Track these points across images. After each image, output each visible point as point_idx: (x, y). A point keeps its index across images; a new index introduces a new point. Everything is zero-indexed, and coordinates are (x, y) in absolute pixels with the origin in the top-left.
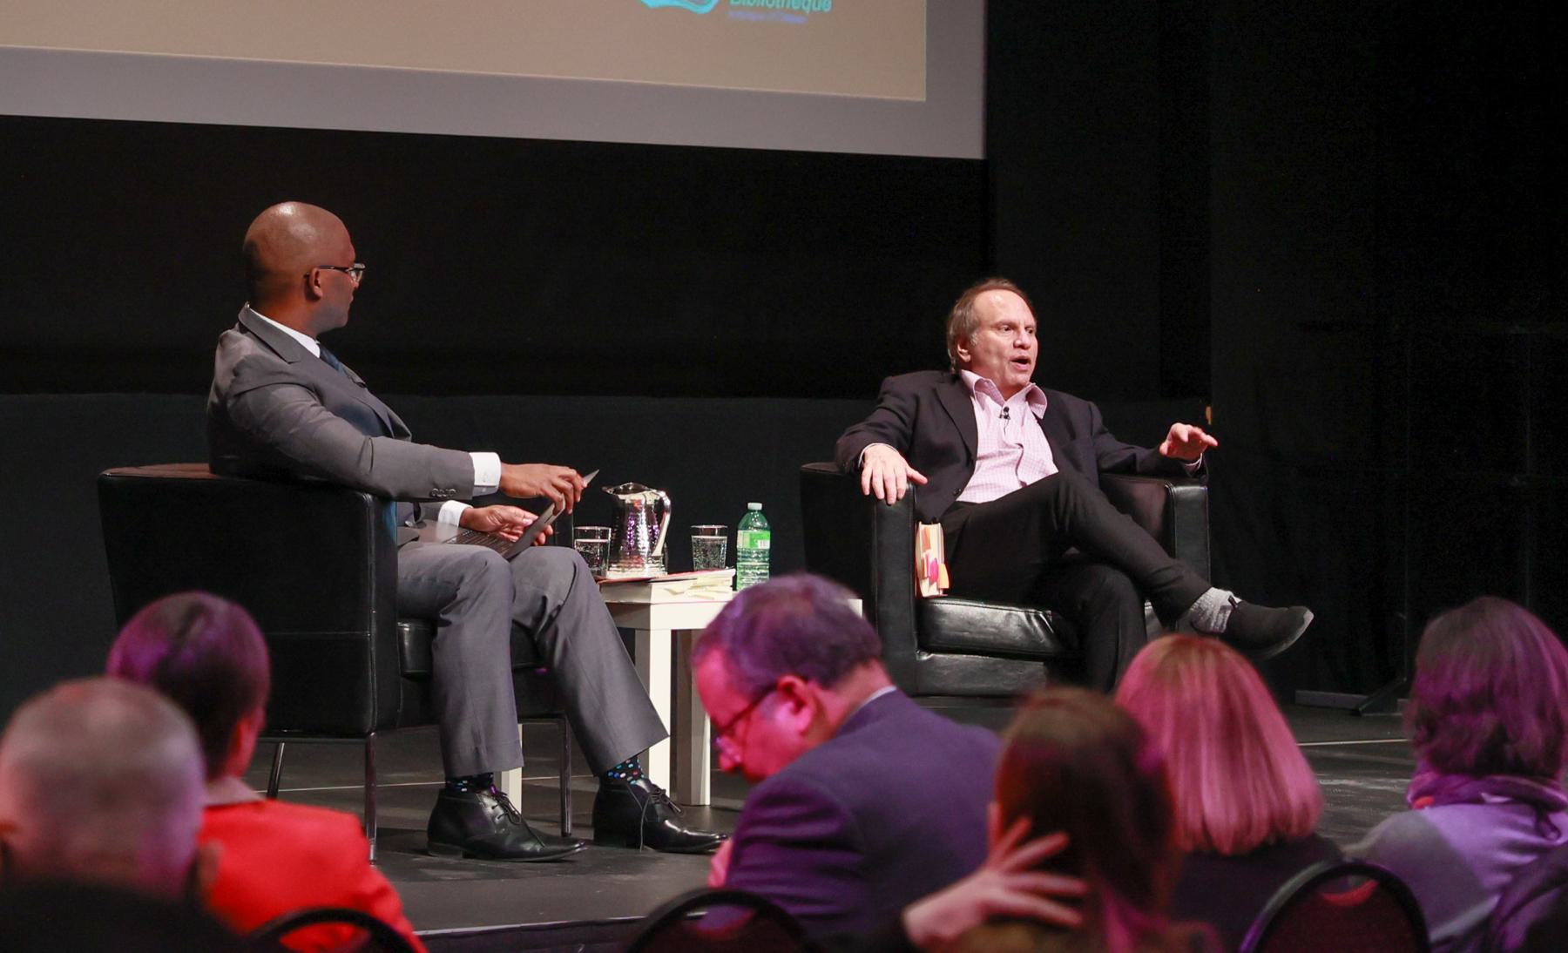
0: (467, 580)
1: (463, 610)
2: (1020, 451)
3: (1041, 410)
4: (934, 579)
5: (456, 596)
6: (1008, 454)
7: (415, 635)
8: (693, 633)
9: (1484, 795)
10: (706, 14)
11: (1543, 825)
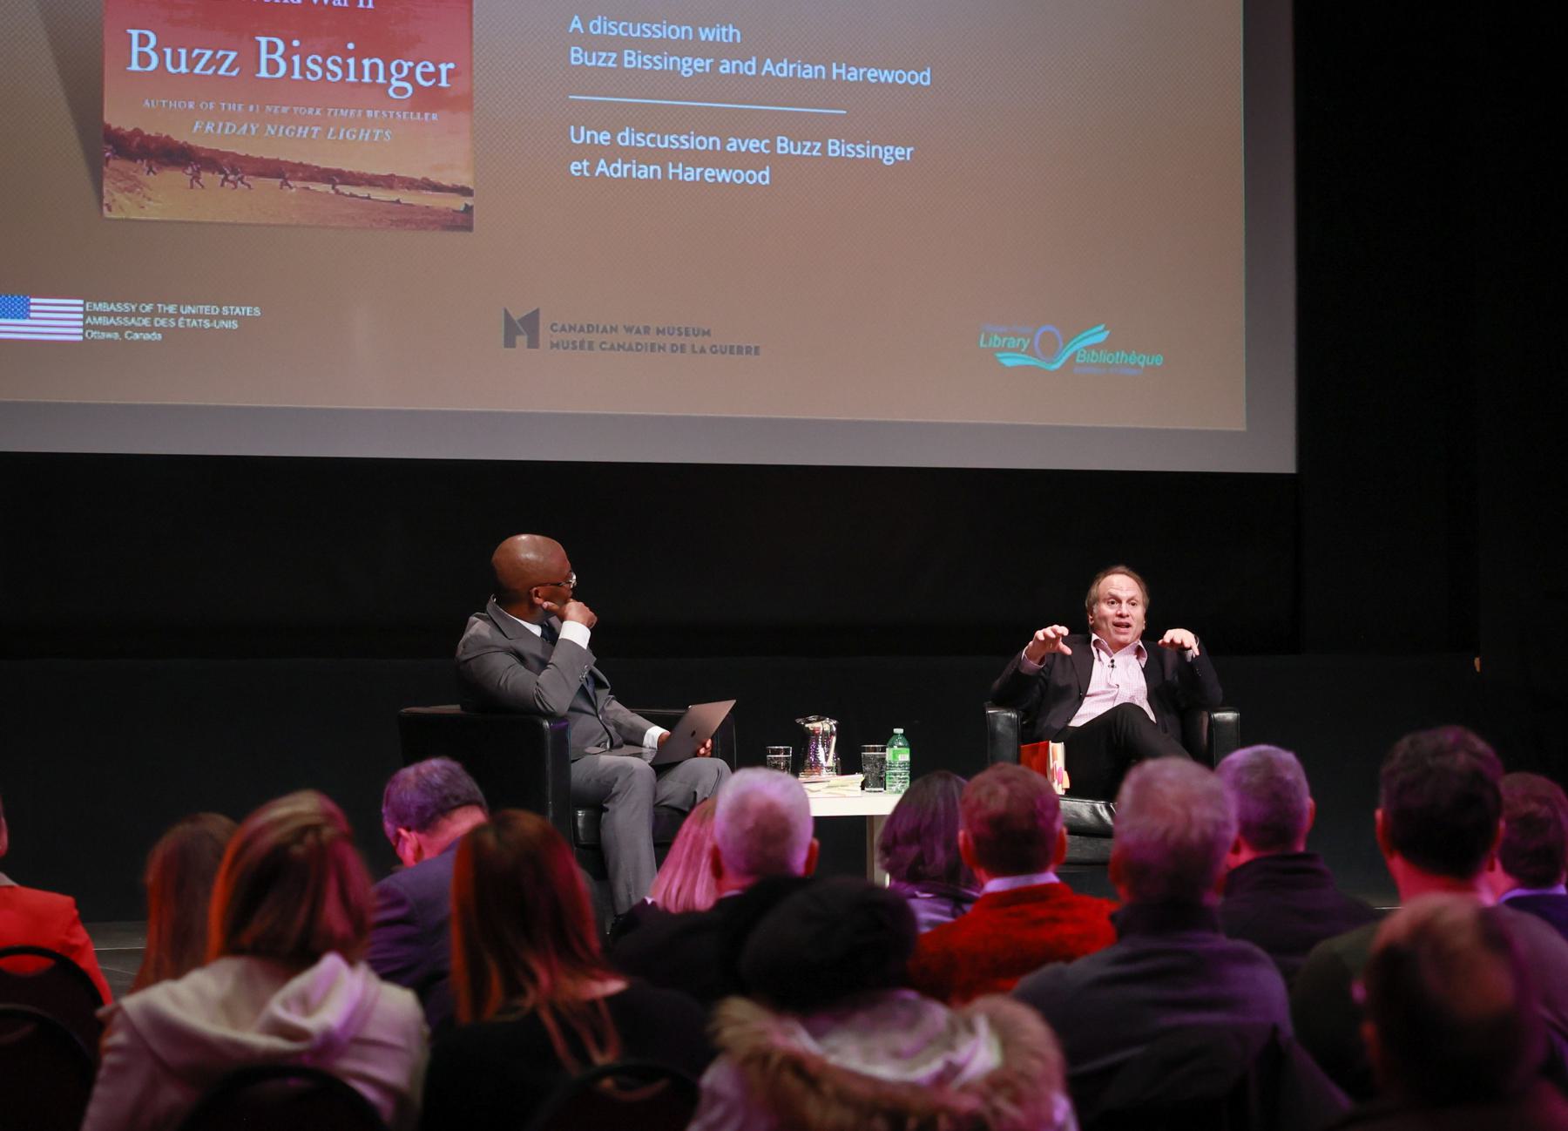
0: (620, 780)
1: (617, 800)
2: (1117, 690)
3: (1144, 661)
4: (1060, 782)
5: (611, 791)
6: (1109, 692)
7: (586, 819)
8: (875, 818)
9: (917, 893)
10: (1057, 371)
11: (958, 911)
